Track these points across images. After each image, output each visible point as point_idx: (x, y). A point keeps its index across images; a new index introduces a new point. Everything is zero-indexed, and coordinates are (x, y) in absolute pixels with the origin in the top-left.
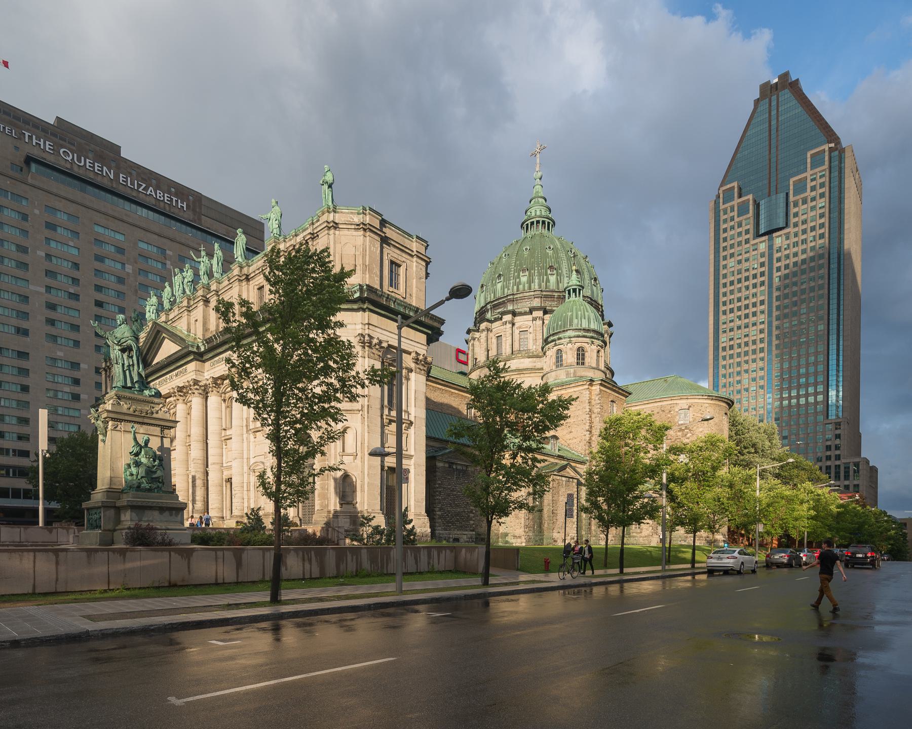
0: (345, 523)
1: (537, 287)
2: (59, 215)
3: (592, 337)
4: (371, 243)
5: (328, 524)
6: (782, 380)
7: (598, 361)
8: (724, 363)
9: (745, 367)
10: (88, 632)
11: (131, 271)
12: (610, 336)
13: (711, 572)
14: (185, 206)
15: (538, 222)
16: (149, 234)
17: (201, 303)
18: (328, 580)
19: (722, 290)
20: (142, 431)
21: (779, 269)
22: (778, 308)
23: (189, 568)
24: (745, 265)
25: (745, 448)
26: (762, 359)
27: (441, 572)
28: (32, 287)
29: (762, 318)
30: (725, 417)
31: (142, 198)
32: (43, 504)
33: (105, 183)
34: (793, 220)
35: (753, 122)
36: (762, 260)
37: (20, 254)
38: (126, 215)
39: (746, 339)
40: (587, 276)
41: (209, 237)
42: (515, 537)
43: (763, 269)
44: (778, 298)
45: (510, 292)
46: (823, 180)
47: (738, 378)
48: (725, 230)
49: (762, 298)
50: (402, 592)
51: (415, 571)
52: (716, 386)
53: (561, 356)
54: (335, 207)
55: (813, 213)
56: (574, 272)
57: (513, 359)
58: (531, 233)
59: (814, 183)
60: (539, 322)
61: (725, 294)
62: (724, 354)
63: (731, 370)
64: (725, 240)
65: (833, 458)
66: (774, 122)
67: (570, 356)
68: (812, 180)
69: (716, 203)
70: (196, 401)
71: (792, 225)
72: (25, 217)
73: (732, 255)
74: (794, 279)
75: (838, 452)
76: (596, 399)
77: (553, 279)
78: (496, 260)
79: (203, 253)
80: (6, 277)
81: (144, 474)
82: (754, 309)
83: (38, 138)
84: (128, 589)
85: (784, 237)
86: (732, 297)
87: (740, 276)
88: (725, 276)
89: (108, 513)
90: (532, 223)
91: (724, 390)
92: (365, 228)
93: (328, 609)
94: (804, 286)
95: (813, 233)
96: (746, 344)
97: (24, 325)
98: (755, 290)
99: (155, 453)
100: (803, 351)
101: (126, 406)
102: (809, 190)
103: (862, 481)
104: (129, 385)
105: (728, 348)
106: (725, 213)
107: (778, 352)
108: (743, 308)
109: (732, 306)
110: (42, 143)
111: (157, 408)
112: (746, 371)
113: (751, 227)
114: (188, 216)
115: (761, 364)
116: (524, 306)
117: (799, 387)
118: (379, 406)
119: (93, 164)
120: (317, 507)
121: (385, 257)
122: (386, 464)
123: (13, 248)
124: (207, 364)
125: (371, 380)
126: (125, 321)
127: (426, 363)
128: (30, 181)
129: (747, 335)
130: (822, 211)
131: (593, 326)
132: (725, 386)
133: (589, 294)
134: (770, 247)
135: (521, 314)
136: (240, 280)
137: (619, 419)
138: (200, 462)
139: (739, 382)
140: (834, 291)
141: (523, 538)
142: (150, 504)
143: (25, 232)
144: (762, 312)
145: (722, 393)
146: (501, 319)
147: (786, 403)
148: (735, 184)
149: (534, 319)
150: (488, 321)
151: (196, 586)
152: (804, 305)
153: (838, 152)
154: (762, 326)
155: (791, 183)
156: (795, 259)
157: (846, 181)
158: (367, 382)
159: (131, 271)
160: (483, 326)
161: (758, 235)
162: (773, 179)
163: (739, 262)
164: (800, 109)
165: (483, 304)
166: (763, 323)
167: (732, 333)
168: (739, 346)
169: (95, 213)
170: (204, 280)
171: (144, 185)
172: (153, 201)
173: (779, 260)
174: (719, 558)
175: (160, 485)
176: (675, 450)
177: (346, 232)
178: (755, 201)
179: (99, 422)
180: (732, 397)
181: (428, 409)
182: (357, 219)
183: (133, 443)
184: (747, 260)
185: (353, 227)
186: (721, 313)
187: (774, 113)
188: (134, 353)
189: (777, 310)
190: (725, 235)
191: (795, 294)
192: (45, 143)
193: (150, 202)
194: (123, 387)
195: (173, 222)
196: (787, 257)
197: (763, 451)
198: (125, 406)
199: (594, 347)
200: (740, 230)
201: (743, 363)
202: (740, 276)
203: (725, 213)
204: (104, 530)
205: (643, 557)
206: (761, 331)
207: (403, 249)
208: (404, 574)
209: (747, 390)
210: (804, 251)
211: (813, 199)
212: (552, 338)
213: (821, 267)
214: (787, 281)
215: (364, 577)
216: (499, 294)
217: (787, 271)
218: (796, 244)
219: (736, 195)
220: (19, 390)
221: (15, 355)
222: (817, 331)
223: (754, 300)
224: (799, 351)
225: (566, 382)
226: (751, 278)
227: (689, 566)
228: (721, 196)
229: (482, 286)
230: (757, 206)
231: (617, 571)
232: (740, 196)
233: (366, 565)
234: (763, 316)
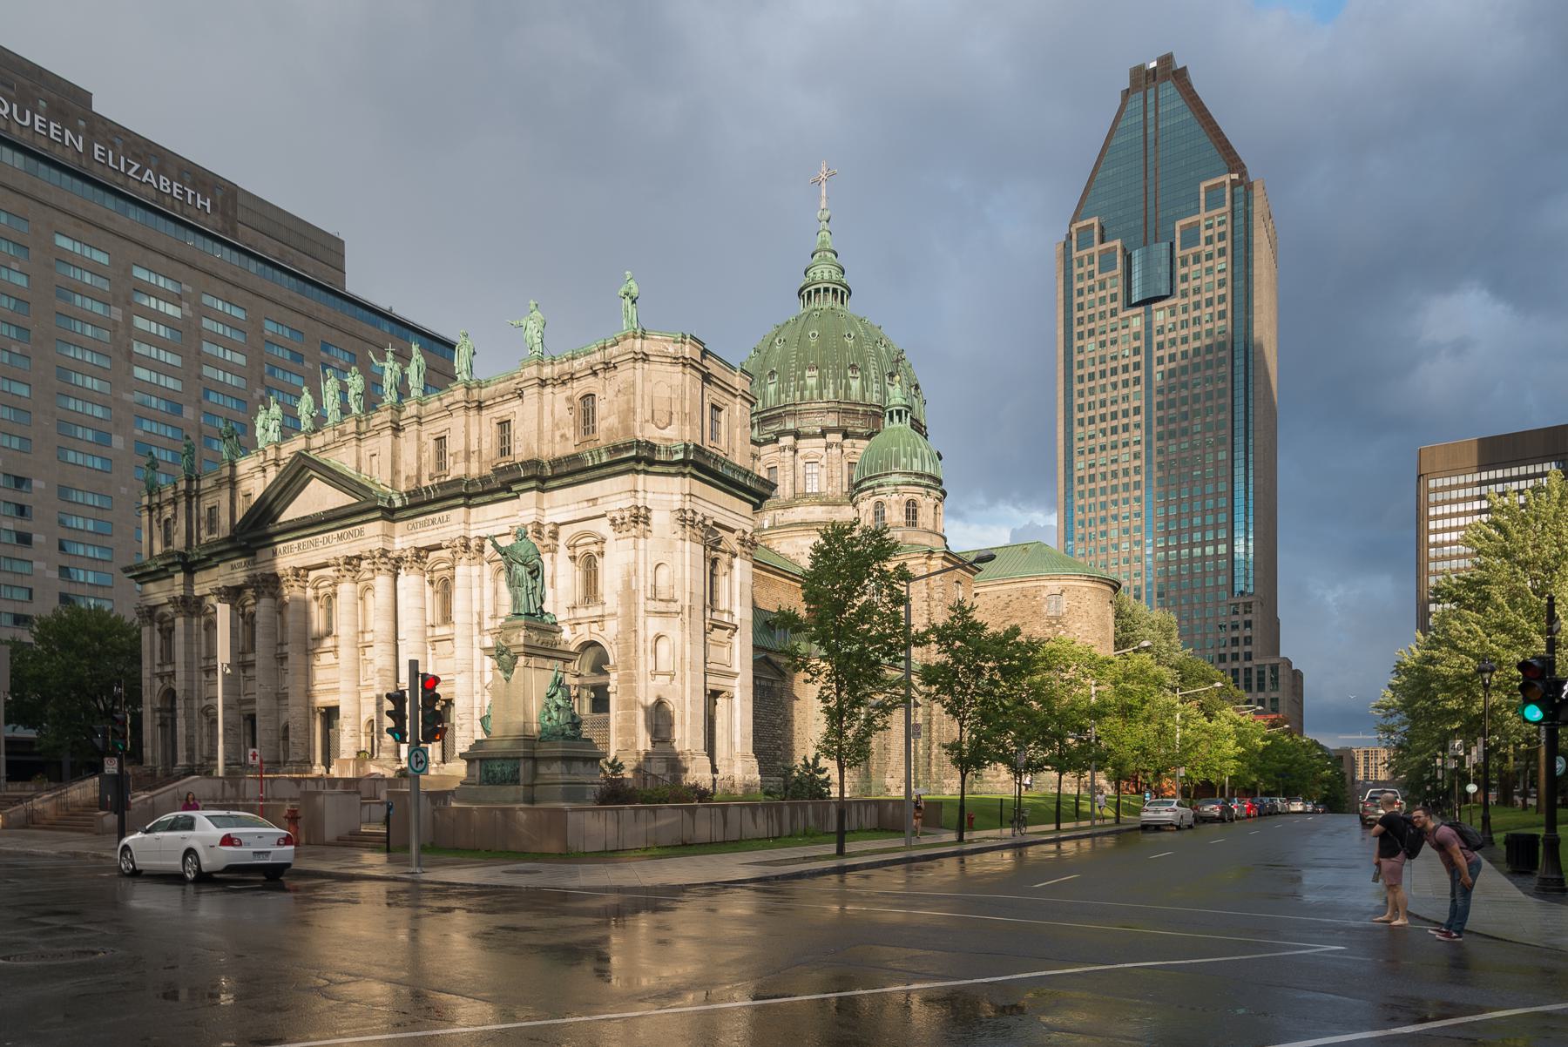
0: (658, 768)
1: (831, 396)
3: (928, 486)
4: (687, 381)
8: (1082, 502)
9: (1113, 510)
11: (120, 319)
14: (208, 205)
15: (826, 290)
16: (152, 256)
17: (389, 432)
21: (1160, 361)
22: (1160, 421)
24: (1111, 350)
26: (1138, 499)
29: (1137, 435)
33: (69, 159)
34: (1181, 286)
36: (1137, 344)
39: (1114, 467)
41: (406, 331)
43: (1137, 359)
44: (1160, 406)
46: (1222, 229)
47: (1103, 528)
49: (1137, 404)
50: (912, 848)
55: (1209, 279)
58: (815, 304)
59: (1209, 232)
61: (1081, 394)
62: (1081, 487)
64: (1081, 307)
65: (1241, 657)
66: (1151, 130)
67: (896, 513)
68: (1209, 227)
69: (1067, 246)
70: (382, 582)
73: (1092, 333)
74: (1184, 378)
75: (1248, 649)
77: (855, 385)
79: (389, 355)
82: (1126, 421)
85: (1168, 311)
86: (1092, 398)
87: (1103, 367)
88: (1081, 365)
92: (686, 363)
94: (1197, 391)
95: (1210, 310)
96: (1115, 474)
98: (1126, 391)
100: (1197, 491)
102: (1203, 242)
103: (1282, 694)
112: (1115, 517)
113: (1119, 290)
115: (1136, 507)
116: (813, 424)
121: (706, 400)
124: (400, 526)
130: (1222, 276)
134: (1148, 325)
136: (467, 408)
139: (1104, 534)
140: (1240, 401)
144: (1137, 426)
145: (1113, 575)
146: (776, 441)
148: (1095, 221)
152: (1198, 420)
153: (1244, 187)
154: (1137, 448)
156: (1185, 347)
157: (1256, 233)
159: (120, 319)
161: (1130, 305)
164: (1189, 115)
166: (1139, 442)
167: (1093, 456)
168: (1104, 476)
169: (57, 213)
170: (390, 397)
171: (137, 166)
172: (154, 193)
173: (1161, 346)
174: (1156, 811)
177: (658, 366)
178: (1124, 250)
184: (1114, 342)
186: (1076, 423)
187: (1151, 115)
190: (1081, 299)
191: (1184, 401)
196: (1173, 342)
199: (930, 500)
200: (1103, 293)
203: (1081, 265)
206: (1136, 456)
207: (726, 388)
209: (1117, 547)
210: (1197, 336)
211: (1209, 257)
212: (867, 484)
213: (1221, 362)
214: (1173, 380)
216: (771, 402)
218: (1185, 324)
219: (1096, 238)
222: (1216, 461)
223: (1125, 406)
228: (1074, 237)
230: (1128, 259)
231: (832, 849)
232: (1102, 241)
234: (1138, 432)
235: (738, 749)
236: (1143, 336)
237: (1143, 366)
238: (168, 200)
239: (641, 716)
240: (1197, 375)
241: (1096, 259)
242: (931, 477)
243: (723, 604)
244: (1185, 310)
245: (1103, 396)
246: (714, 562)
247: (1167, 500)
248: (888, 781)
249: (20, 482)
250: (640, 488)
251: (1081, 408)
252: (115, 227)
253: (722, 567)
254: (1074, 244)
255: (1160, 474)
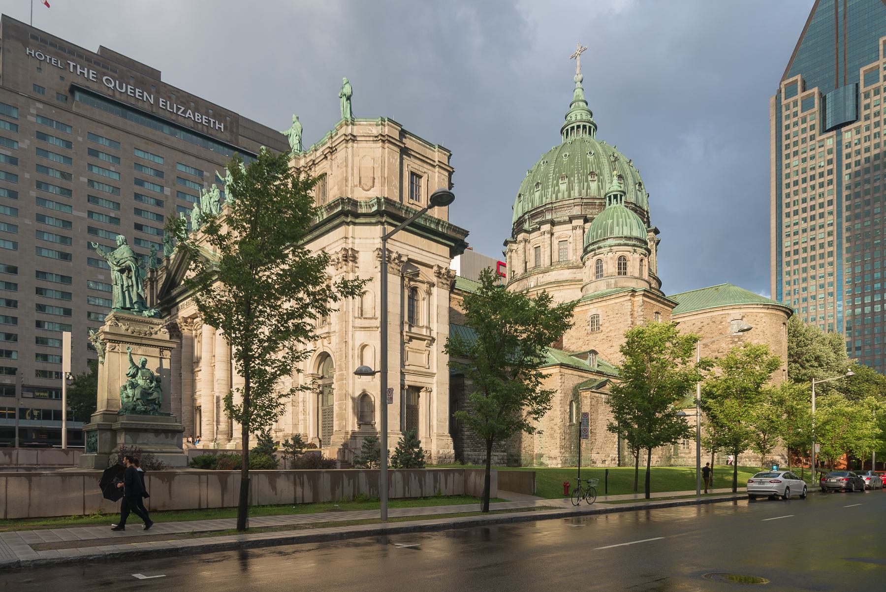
1: (577, 195)
2: (101, 141)
3: (634, 245)
4: (391, 155)
5: (345, 445)
6: (854, 286)
7: (641, 270)
8: (789, 269)
9: (812, 272)
10: (19, 562)
11: (169, 194)
12: (657, 244)
13: (752, 497)
14: (222, 127)
15: (578, 127)
16: (187, 157)
18: (322, 506)
19: (785, 191)
20: (140, 352)
22: (848, 208)
23: (170, 493)
24: (810, 163)
25: (808, 361)
26: (831, 264)
27: (449, 497)
28: (75, 213)
29: (830, 219)
30: (783, 328)
31: (181, 121)
32: (66, 425)
33: (146, 108)
34: (864, 113)
35: (818, 10)
37: (64, 181)
38: (165, 138)
39: (813, 243)
40: (630, 181)
42: (550, 458)
43: (831, 167)
44: (848, 198)
45: (549, 201)
47: (804, 285)
48: (788, 127)
49: (830, 198)
51: (419, 495)
52: (779, 294)
53: (602, 267)
54: (353, 120)
56: (615, 178)
57: (552, 270)
58: (573, 137)
60: (579, 232)
61: (788, 196)
62: (788, 259)
63: (796, 277)
66: (841, 9)
71: (863, 118)
72: (68, 144)
73: (796, 153)
74: (866, 177)
76: (638, 311)
77: (594, 186)
78: (534, 168)
80: (51, 204)
81: (139, 396)
82: (821, 210)
83: (82, 68)
84: (105, 515)
85: (854, 132)
86: (796, 198)
87: (804, 175)
88: (788, 176)
89: (103, 435)
90: (572, 128)
91: (789, 298)
92: (384, 139)
93: (293, 538)
94: (877, 184)
96: (813, 248)
97: (67, 249)
98: (822, 190)
99: (152, 374)
101: (124, 328)
104: (128, 305)
105: (792, 253)
106: (788, 108)
107: (849, 255)
108: (809, 209)
109: (796, 208)
110: (86, 72)
111: (156, 328)
112: (813, 277)
113: (817, 122)
114: (225, 137)
115: (829, 269)
116: (563, 215)
117: (873, 293)
118: (398, 323)
119: (135, 90)
120: (335, 428)
121: (405, 168)
122: (407, 383)
123: (58, 175)
125: (342, 293)
126: (125, 242)
127: (449, 277)
128: (74, 109)
129: (814, 239)
131: (636, 233)
132: (789, 294)
133: (633, 200)
134: (839, 143)
135: (560, 223)
137: (642, 333)
138: (224, 382)
139: (805, 289)
141: (559, 459)
142: (144, 427)
143: (68, 159)
144: (831, 213)
145: (786, 302)
146: (539, 229)
147: (858, 311)
148: (798, 77)
149: (574, 228)
150: (526, 231)
151: (177, 511)
152: (878, 204)
154: (831, 228)
155: (862, 72)
156: (868, 155)
158: (339, 295)
159: (169, 194)
160: (521, 237)
161: (824, 130)
162: (841, 70)
163: (804, 160)
165: (520, 214)
167: (797, 237)
168: (805, 250)
171: (183, 108)
172: (192, 124)
173: (848, 156)
174: (761, 482)
175: (156, 407)
176: (705, 364)
177: (364, 144)
178: (820, 94)
179: (98, 344)
180: (793, 307)
181: (451, 323)
182: (375, 131)
183: (130, 365)
184: (812, 158)
185: (371, 139)
186: (784, 216)
188: (133, 274)
189: (847, 210)
190: (788, 132)
191: (867, 192)
192: (88, 72)
193: (188, 124)
194: (122, 308)
195: (211, 143)
196: (858, 152)
197: (827, 364)
198: (123, 328)
200: (804, 125)
201: (809, 269)
202: (804, 175)
203: (788, 108)
204: (100, 453)
205: (678, 480)
206: (830, 234)
207: (424, 160)
208: (390, 499)
209: (814, 297)
212: (591, 247)
214: (858, 179)
215: (361, 502)
216: (537, 203)
217: (858, 168)
218: (867, 139)
219: (799, 88)
220: (62, 313)
221: (59, 279)
223: (821, 200)
224: (872, 254)
225: (606, 293)
226: (817, 176)
227: (730, 490)
228: (783, 91)
229: (520, 196)
230: (823, 99)
232: (804, 90)
233: (365, 489)
234: (831, 217)
235: (435, 431)
236: (835, 151)
237: (835, 171)
238: (200, 126)
239: (350, 403)
240: (878, 173)
241: (799, 103)
242: (637, 239)
243: (423, 320)
244: (868, 129)
245: (805, 195)
246: (414, 290)
247: (854, 263)
248: (594, 456)
249: (13, 270)
250: (350, 235)
251: (788, 205)
252: (169, 143)
253: (421, 294)
254: (783, 95)
255: (848, 245)
